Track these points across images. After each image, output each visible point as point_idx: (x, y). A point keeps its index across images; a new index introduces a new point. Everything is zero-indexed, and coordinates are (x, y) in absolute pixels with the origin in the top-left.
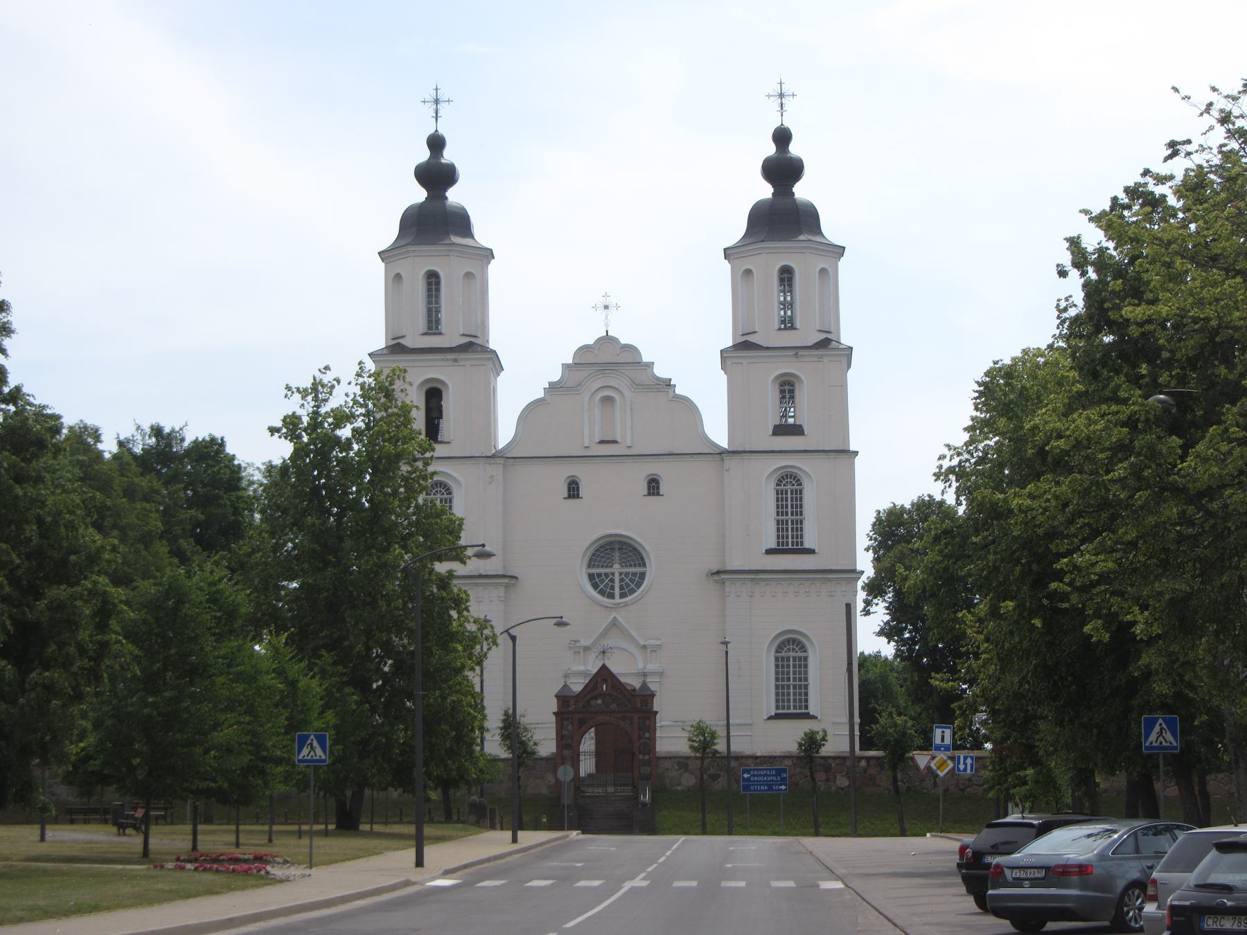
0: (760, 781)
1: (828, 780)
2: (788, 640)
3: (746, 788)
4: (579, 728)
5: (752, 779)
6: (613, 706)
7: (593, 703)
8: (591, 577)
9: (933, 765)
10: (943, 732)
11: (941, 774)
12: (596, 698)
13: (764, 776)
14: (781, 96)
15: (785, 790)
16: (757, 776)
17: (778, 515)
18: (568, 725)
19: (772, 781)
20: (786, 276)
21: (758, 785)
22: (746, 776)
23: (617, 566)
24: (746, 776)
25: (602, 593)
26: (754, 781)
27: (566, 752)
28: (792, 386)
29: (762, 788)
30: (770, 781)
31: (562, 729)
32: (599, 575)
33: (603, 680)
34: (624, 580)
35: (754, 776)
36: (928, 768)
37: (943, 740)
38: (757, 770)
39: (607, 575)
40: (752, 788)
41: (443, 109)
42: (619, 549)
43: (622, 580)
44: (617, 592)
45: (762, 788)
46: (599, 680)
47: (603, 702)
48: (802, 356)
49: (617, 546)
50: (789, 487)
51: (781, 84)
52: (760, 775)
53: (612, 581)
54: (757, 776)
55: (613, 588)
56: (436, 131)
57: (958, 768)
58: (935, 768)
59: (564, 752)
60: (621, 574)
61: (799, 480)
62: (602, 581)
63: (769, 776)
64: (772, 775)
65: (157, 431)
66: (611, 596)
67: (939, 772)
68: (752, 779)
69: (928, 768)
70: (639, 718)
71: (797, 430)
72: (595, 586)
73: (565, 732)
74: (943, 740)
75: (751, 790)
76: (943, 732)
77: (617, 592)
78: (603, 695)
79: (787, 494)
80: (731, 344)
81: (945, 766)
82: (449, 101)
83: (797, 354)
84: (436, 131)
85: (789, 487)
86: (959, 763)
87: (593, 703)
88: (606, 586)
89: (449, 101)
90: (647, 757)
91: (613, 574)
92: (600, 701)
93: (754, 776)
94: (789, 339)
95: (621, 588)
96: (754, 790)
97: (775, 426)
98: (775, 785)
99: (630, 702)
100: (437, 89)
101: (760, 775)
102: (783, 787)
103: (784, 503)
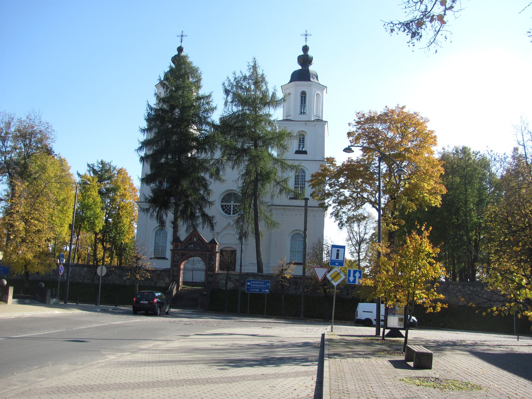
0: (256, 287)
1: (296, 289)
2: (297, 233)
3: (248, 289)
4: (182, 258)
5: (252, 285)
6: (198, 248)
7: (189, 246)
8: (222, 206)
9: (328, 276)
10: (338, 251)
11: (335, 284)
12: (190, 244)
13: (258, 284)
14: (306, 35)
15: (268, 292)
16: (254, 284)
17: (295, 184)
18: (177, 256)
19: (262, 287)
20: (303, 95)
21: (254, 289)
22: (248, 283)
23: (232, 202)
24: (248, 283)
25: (226, 212)
26: (252, 287)
27: (175, 268)
28: (304, 136)
29: (257, 290)
30: (261, 287)
31: (174, 258)
32: (225, 206)
33: (194, 236)
34: (235, 208)
35: (253, 284)
36: (325, 278)
37: (337, 257)
38: (254, 281)
39: (228, 206)
40: (251, 290)
41: (184, 38)
42: (234, 196)
43: (234, 208)
44: (232, 212)
45: (257, 290)
46: (193, 236)
47: (194, 246)
48: (308, 124)
49: (233, 195)
50: (300, 174)
51: (306, 31)
52: (256, 284)
53: (230, 208)
54: (254, 284)
55: (230, 211)
56: (181, 46)
57: (349, 280)
58: (330, 279)
59: (174, 268)
60: (234, 206)
61: (304, 171)
62: (226, 208)
63: (260, 284)
64: (262, 284)
65: (102, 163)
66: (230, 214)
67: (333, 282)
68: (252, 285)
69: (325, 278)
70: (209, 254)
71: (305, 153)
72: (223, 210)
73: (175, 259)
74: (337, 257)
75: (251, 291)
76: (338, 251)
77: (232, 212)
78: (194, 243)
79: (299, 176)
80: (282, 119)
81: (339, 276)
82: (186, 36)
83: (306, 123)
84: (181, 46)
85: (300, 174)
86: (349, 276)
87: (189, 246)
88: (228, 210)
89: (182, 32)
90: (212, 273)
91: (231, 205)
92: (192, 246)
93: (253, 284)
94: (303, 117)
95: (233, 211)
96: (252, 291)
97: (296, 151)
98: (263, 289)
99: (206, 247)
100: (182, 32)
101: (256, 284)
102: (267, 291)
103: (298, 180)
